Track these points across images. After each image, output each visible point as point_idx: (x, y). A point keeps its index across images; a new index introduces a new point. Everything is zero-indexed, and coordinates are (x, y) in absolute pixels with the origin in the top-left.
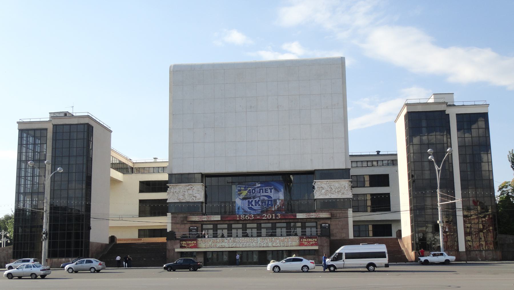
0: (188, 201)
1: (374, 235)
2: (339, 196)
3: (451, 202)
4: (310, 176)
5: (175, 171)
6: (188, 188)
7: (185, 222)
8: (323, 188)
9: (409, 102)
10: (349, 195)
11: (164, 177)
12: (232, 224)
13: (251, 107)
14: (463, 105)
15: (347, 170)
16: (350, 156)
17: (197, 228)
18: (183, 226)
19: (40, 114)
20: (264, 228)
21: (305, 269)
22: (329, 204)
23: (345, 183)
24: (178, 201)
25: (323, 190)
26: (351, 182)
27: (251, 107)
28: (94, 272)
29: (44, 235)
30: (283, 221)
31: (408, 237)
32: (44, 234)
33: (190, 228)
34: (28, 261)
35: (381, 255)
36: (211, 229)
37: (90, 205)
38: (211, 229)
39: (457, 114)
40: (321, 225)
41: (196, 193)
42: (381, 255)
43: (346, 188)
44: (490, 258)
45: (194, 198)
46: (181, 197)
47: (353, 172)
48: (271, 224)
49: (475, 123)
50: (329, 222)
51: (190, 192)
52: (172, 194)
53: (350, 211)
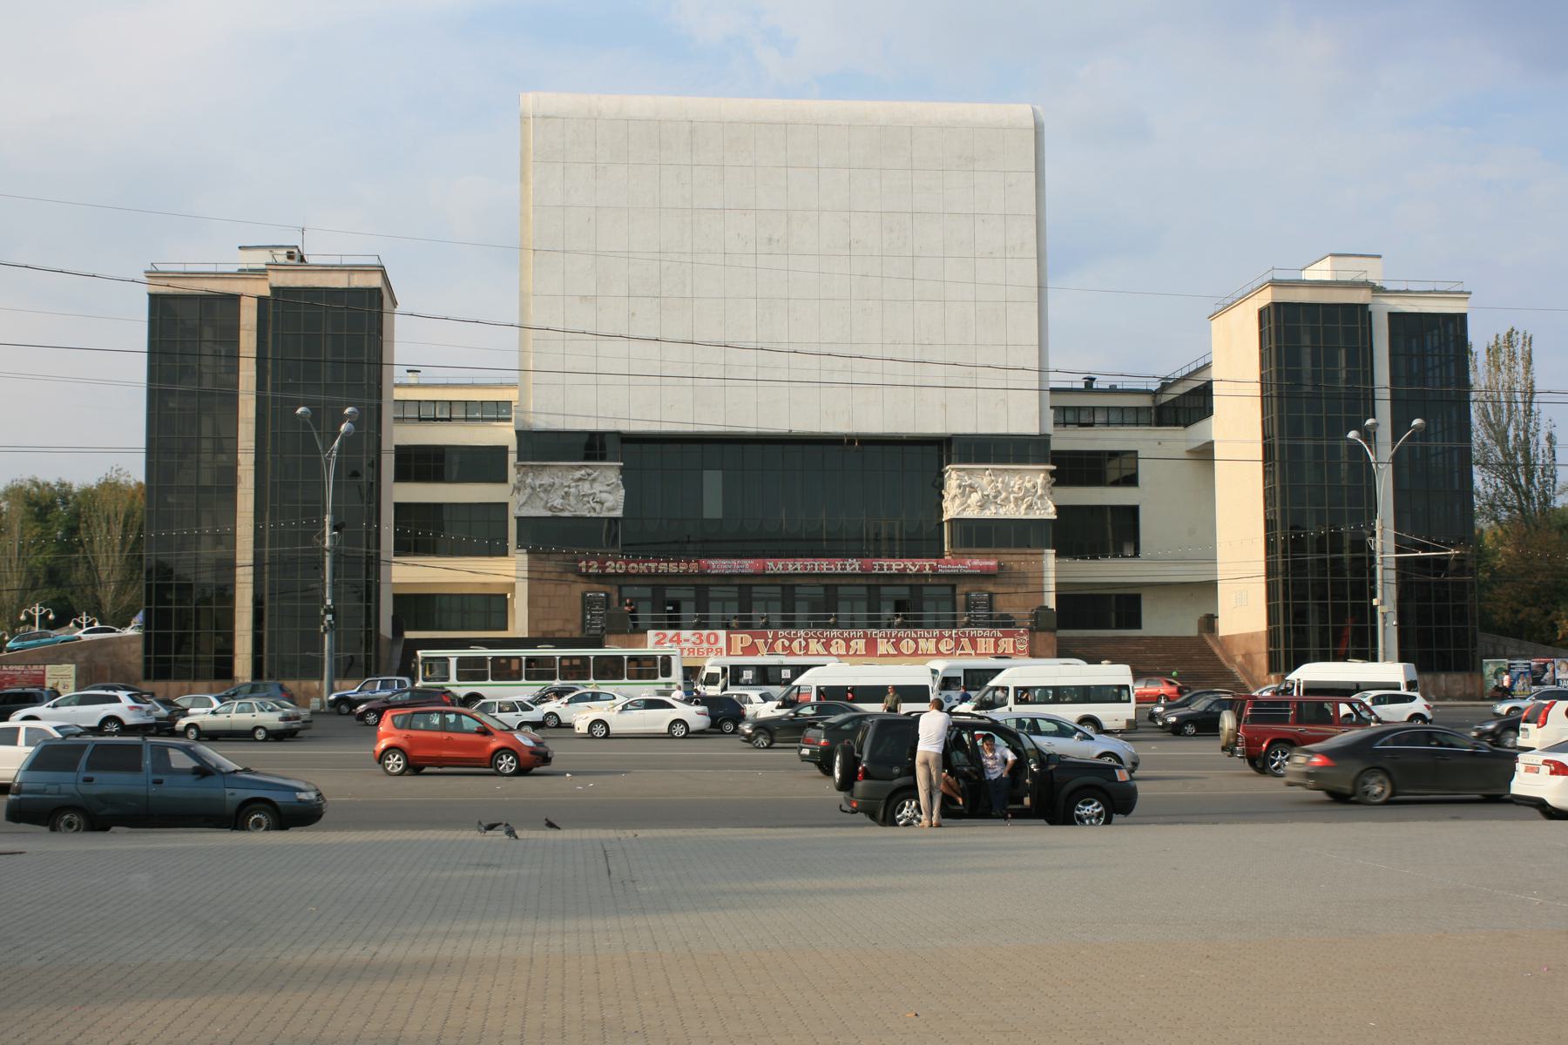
1: (400, 508)
2: (1021, 514)
4: (939, 451)
5: (541, 423)
6: (578, 474)
9: (1279, 276)
10: (1049, 512)
11: (502, 435)
14: (1407, 291)
17: (608, 595)
18: (563, 590)
19: (221, 248)
22: (978, 533)
23: (1035, 477)
24: (549, 514)
25: (966, 495)
26: (1052, 473)
28: (265, 740)
29: (329, 617)
32: (326, 612)
33: (584, 595)
34: (116, 700)
35: (1115, 694)
37: (1267, 553)
38: (776, 599)
39: (1390, 314)
40: (967, 594)
41: (601, 492)
42: (1115, 694)
45: (598, 507)
46: (558, 502)
47: (1056, 445)
48: (779, 589)
50: (992, 589)
51: (585, 487)
52: (528, 491)
53: (1050, 558)
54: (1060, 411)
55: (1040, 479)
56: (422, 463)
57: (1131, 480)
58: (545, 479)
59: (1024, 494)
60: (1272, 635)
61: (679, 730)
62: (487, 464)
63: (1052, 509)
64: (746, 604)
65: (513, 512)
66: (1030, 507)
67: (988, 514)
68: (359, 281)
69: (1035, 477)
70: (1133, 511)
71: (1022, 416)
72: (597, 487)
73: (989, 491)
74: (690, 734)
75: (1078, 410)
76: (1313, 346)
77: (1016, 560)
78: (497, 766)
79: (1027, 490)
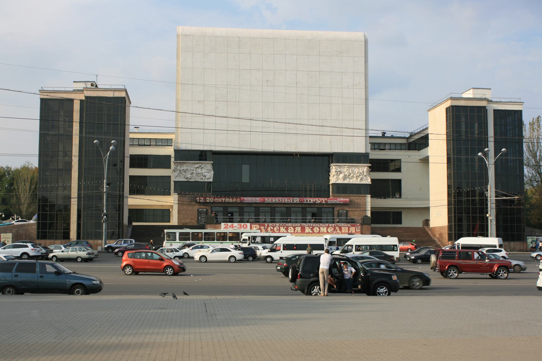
0: (196, 180)
1: (132, 178)
2: (358, 182)
3: (504, 198)
4: (330, 158)
5: (183, 147)
6: (196, 166)
7: (194, 203)
8: (341, 172)
10: (368, 181)
11: (169, 151)
12: (243, 207)
13: (267, 81)
15: (366, 155)
16: (370, 137)
17: (207, 210)
18: (191, 208)
20: (278, 212)
21: (186, 256)
23: (364, 168)
24: (186, 180)
25: (338, 174)
27: (267, 81)
29: (105, 217)
30: (298, 206)
31: (442, 228)
32: (104, 215)
33: (198, 210)
36: (236, 212)
39: (494, 110)
40: (338, 211)
41: (205, 172)
43: (365, 174)
44: (518, 249)
45: (203, 178)
46: (189, 176)
48: (269, 208)
49: (510, 122)
51: (199, 171)
52: (178, 171)
53: (369, 198)
54: (373, 144)
55: (365, 169)
56: (139, 161)
57: (399, 170)
58: (185, 167)
59: (359, 174)
60: (450, 227)
61: (233, 260)
62: (163, 162)
63: (370, 180)
64: (257, 214)
65: (173, 179)
66: (361, 179)
67: (346, 182)
68: (117, 94)
69: (364, 168)
70: (399, 181)
71: (359, 146)
72: (204, 171)
73: (347, 173)
74: (236, 261)
75: (379, 144)
76: (465, 121)
77: (356, 199)
78: (166, 272)
79: (361, 173)
